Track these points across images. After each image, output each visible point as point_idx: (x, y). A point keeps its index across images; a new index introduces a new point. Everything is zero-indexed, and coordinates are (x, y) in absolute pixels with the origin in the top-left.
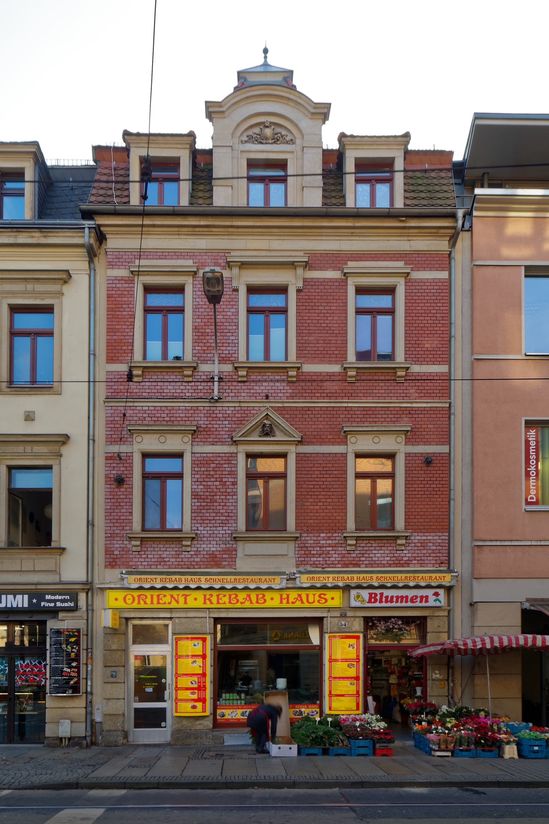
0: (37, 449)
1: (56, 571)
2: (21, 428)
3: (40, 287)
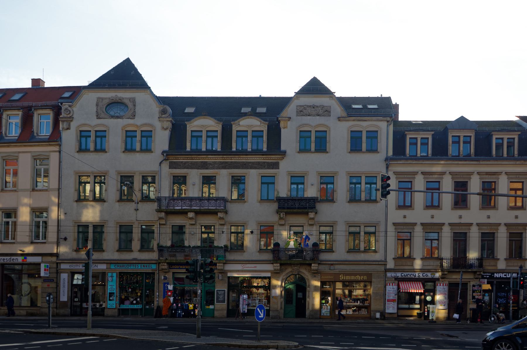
0: (520, 227)
1: (496, 266)
2: (457, 221)
3: (520, 176)
